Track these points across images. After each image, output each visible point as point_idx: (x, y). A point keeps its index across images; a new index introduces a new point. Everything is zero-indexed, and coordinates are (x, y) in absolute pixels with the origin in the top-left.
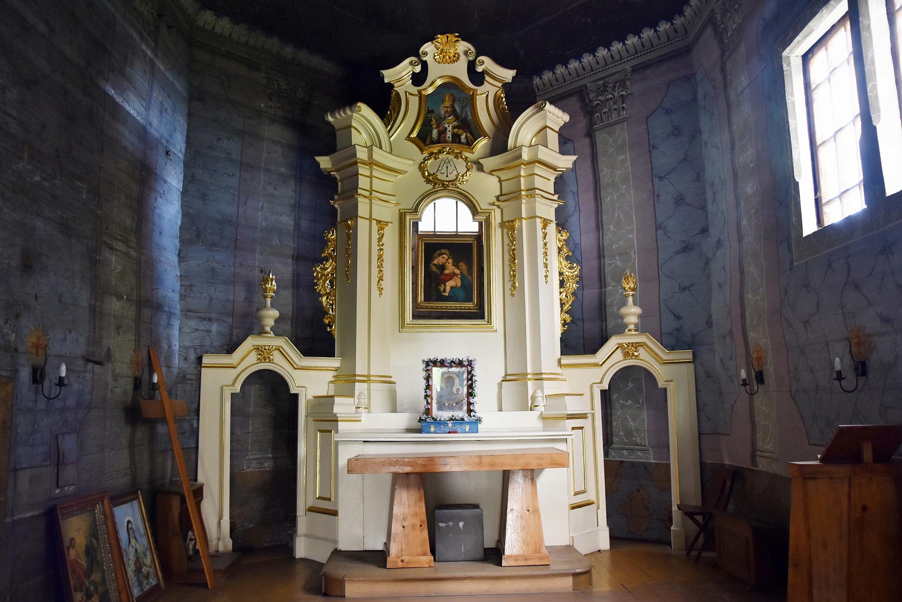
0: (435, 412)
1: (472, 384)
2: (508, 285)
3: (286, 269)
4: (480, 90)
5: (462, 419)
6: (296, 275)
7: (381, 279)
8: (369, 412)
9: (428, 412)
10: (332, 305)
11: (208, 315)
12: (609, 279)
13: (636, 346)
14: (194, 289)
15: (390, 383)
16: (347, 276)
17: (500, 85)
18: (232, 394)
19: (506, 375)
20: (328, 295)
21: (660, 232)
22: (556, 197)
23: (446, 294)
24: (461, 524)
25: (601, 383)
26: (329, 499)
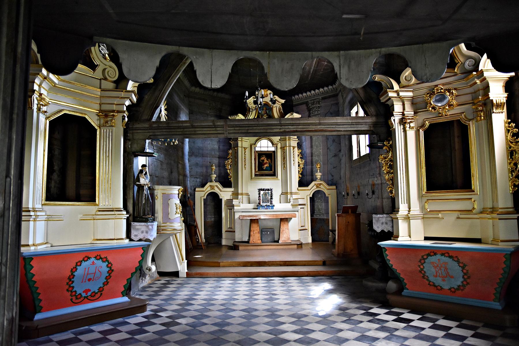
0: (261, 204)
1: (272, 196)
2: (283, 166)
3: (216, 161)
4: (274, 106)
5: (269, 205)
6: (219, 163)
7: (245, 165)
8: (243, 204)
9: (259, 203)
10: (231, 172)
11: (196, 177)
12: (314, 164)
13: (320, 184)
14: (193, 169)
15: (248, 195)
16: (235, 164)
17: (280, 104)
18: (204, 199)
19: (282, 193)
20: (229, 169)
21: (328, 150)
22: (297, 140)
23: (264, 169)
24: (269, 233)
25: (310, 195)
26: (232, 228)
